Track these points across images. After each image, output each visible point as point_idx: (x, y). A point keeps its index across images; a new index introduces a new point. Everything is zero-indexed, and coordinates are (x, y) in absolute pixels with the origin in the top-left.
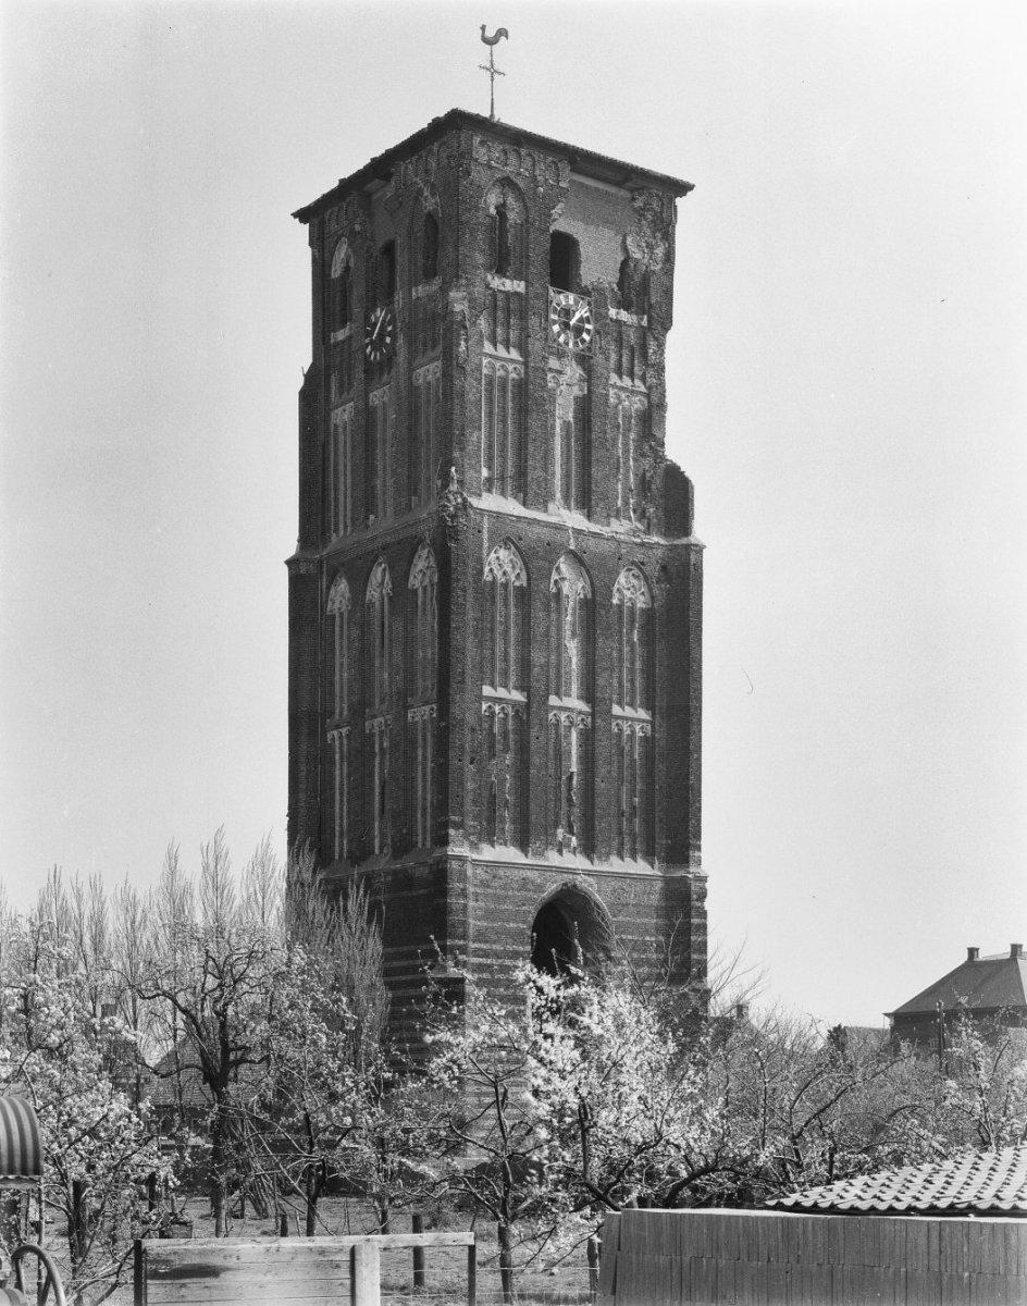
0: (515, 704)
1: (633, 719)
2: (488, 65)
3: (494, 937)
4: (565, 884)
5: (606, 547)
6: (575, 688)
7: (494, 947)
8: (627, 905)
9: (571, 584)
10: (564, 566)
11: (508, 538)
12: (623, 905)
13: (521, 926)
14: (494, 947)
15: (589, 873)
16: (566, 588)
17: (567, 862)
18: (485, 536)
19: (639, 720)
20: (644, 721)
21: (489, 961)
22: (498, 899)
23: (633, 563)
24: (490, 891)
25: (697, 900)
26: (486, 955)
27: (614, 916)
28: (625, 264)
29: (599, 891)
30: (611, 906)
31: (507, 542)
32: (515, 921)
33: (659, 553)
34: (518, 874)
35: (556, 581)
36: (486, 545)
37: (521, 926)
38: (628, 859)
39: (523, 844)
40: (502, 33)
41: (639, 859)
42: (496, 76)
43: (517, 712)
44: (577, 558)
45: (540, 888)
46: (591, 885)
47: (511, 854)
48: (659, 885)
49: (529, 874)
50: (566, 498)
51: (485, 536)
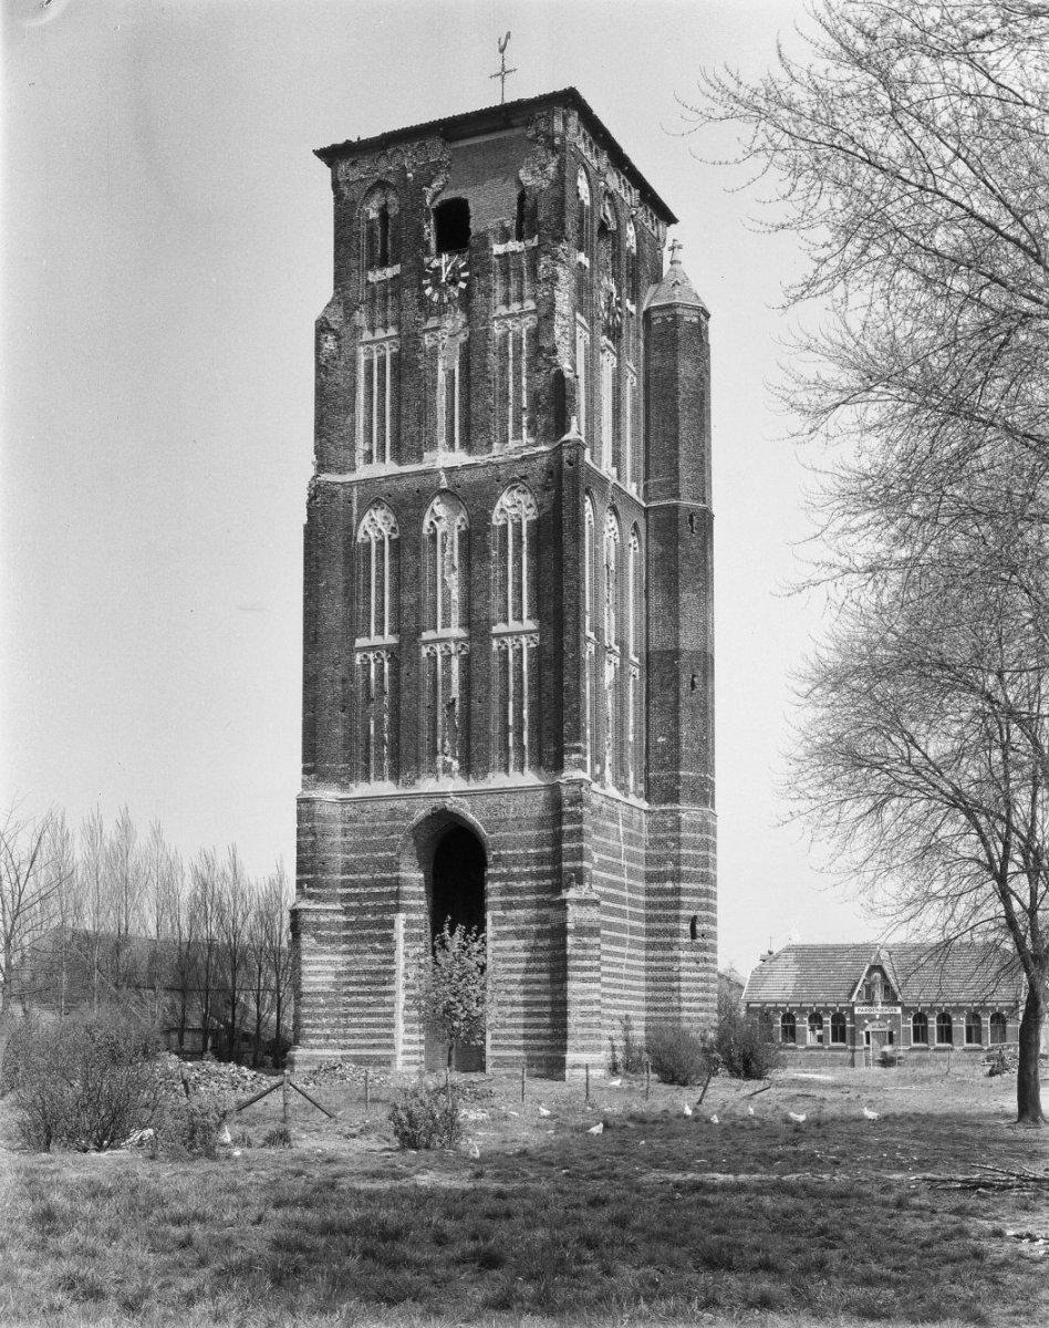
0: (388, 648)
1: (519, 633)
2: (499, 78)
3: (360, 868)
4: (435, 808)
5: (480, 475)
6: (455, 618)
7: (362, 876)
8: (506, 819)
9: (443, 520)
10: (439, 507)
11: (378, 499)
12: (501, 821)
13: (390, 854)
14: (362, 876)
15: (460, 794)
16: (441, 527)
17: (444, 785)
18: (355, 504)
19: (524, 632)
20: (531, 632)
21: (357, 891)
22: (365, 832)
23: (514, 480)
24: (358, 825)
25: (570, 805)
26: (353, 884)
27: (492, 833)
28: (522, 198)
29: (472, 811)
30: (487, 823)
31: (376, 502)
32: (382, 850)
33: (545, 461)
34: (384, 806)
35: (432, 523)
36: (355, 511)
37: (390, 854)
38: (472, 781)
39: (395, 775)
40: (680, 247)
41: (526, 769)
42: (499, 78)
43: (392, 654)
44: (449, 495)
45: (408, 815)
46: (462, 806)
47: (386, 787)
48: (542, 795)
49: (396, 804)
50: (451, 441)
51: (355, 504)
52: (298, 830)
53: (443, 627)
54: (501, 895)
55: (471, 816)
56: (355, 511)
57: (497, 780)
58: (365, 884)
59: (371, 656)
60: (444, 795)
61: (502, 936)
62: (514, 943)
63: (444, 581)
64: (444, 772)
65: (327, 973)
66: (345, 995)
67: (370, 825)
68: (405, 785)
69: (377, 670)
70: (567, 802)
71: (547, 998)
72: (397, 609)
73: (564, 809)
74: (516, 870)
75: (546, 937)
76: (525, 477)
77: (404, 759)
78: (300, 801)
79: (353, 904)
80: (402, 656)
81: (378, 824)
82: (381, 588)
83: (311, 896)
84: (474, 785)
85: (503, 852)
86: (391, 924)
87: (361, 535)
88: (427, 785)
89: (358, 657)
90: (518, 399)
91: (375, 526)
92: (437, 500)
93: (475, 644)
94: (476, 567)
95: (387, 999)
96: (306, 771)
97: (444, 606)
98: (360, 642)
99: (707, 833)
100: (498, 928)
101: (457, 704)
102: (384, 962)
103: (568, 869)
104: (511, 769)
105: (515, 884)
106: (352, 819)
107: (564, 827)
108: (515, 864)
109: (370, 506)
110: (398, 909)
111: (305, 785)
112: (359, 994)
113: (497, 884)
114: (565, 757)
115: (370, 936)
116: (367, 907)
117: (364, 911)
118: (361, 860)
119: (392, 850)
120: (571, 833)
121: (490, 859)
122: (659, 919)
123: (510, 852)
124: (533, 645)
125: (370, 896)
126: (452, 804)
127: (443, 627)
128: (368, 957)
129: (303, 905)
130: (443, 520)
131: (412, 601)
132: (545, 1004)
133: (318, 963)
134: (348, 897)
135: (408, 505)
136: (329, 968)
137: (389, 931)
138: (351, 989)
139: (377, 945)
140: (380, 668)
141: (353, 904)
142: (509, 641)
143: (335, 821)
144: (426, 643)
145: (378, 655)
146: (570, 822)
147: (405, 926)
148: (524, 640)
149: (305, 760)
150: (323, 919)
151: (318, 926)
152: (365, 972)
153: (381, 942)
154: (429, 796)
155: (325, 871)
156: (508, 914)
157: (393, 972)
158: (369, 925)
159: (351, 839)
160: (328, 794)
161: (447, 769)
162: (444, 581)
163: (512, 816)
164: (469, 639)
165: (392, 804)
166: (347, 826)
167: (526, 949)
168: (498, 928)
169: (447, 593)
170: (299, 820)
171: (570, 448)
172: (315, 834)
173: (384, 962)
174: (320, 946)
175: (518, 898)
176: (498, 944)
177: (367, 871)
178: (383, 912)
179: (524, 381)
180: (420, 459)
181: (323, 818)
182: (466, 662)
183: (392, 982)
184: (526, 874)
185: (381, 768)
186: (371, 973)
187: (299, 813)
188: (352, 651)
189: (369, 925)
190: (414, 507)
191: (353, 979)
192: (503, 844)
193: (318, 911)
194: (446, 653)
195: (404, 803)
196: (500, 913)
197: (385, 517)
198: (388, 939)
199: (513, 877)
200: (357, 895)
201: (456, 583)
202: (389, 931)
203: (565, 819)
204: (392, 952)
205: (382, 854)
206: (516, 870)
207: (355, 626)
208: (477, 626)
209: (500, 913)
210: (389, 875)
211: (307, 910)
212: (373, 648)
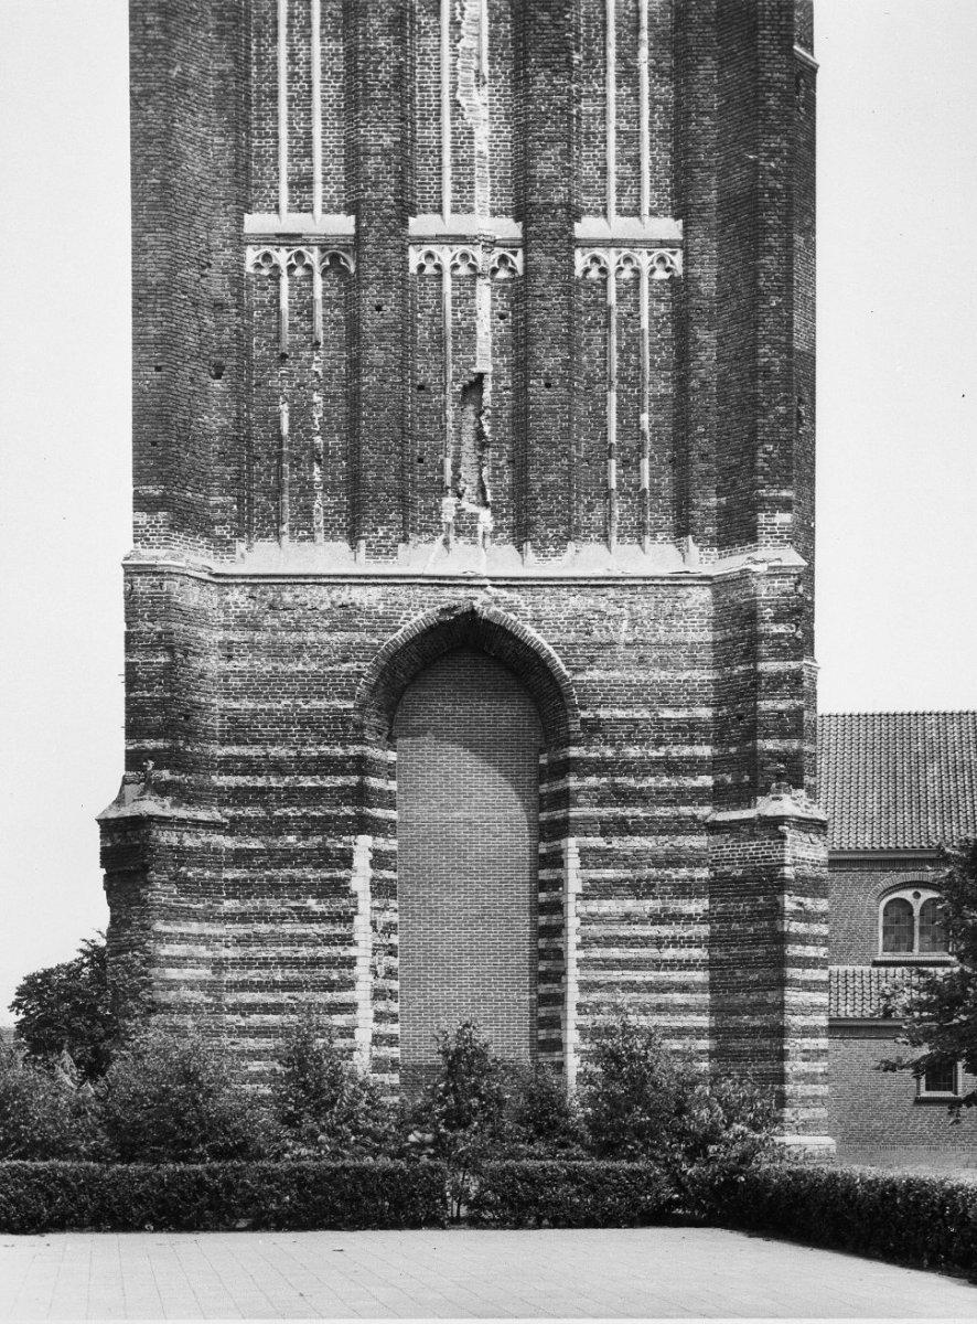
1: (634, 244)
6: (482, 194)
7: (274, 751)
8: (612, 643)
12: (602, 646)
14: (274, 751)
21: (261, 782)
22: (277, 652)
24: (259, 637)
25: (776, 620)
32: (320, 695)
38: (531, 556)
45: (387, 622)
46: (512, 608)
47: (330, 555)
52: (129, 637)
57: (586, 559)
58: (278, 767)
59: (282, 257)
61: (595, 890)
62: (630, 905)
63: (456, 104)
64: (459, 532)
65: (200, 961)
66: (234, 1009)
67: (294, 637)
68: (375, 552)
69: (301, 298)
70: (769, 612)
71: (704, 1021)
72: (353, 155)
73: (762, 628)
74: (633, 752)
75: (700, 895)
77: (380, 492)
78: (132, 571)
79: (249, 812)
80: (366, 264)
81: (311, 637)
83: (162, 789)
84: (532, 565)
85: (603, 713)
86: (346, 860)
88: (423, 557)
89: (251, 255)
93: (539, 257)
94: (541, 81)
95: (339, 1020)
96: (142, 503)
98: (255, 223)
99: (801, 737)
100: (594, 874)
101: (488, 386)
102: (329, 940)
103: (770, 753)
104: (614, 538)
105: (632, 782)
106: (248, 623)
107: (762, 666)
108: (630, 740)
110: (364, 825)
111: (140, 536)
112: (267, 1009)
113: (592, 781)
114: (762, 518)
115: (293, 883)
117: (282, 826)
118: (270, 713)
119: (344, 696)
120: (777, 680)
121: (575, 726)
122: (331, 962)
123: (620, 714)
124: (661, 275)
125: (292, 795)
126: (483, 602)
127: (455, 211)
129: (151, 806)
131: (387, 141)
132: (698, 1033)
133: (183, 938)
134: (240, 796)
136: (202, 951)
137: (341, 874)
138: (248, 997)
139: (312, 903)
140: (302, 290)
141: (249, 812)
142: (611, 258)
143: (205, 624)
144: (421, 241)
145: (300, 255)
146: (777, 656)
147: (373, 864)
148: (644, 260)
149: (140, 475)
150: (189, 842)
151: (182, 855)
152: (283, 963)
153: (319, 896)
155: (190, 734)
156: (616, 843)
157: (350, 963)
158: (289, 857)
159: (243, 665)
160: (190, 556)
162: (456, 104)
163: (624, 637)
164: (525, 244)
166: (235, 637)
167: (706, 918)
168: (594, 874)
169: (464, 137)
170: (131, 615)
172: (170, 650)
173: (329, 940)
174: (185, 902)
175: (639, 812)
176: (594, 907)
177: (281, 739)
178: (324, 831)
181: (189, 616)
182: (519, 293)
183: (349, 985)
184: (656, 762)
185: (307, 512)
186: (296, 963)
187: (131, 599)
188: (239, 241)
189: (289, 857)
191: (252, 975)
192: (608, 697)
193: (182, 822)
194: (463, 270)
195: (376, 593)
196: (597, 842)
198: (339, 888)
199: (627, 767)
201: (484, 113)
202: (341, 874)
203: (763, 650)
204: (348, 919)
205: (322, 704)
206: (633, 752)
207: (246, 189)
208: (541, 214)
209: (597, 842)
210: (339, 751)
211: (164, 821)
212: (287, 239)
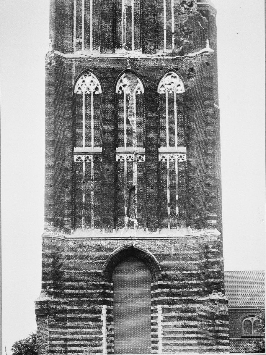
4: (127, 246)
5: (151, 65)
9: (130, 88)
12: (167, 255)
21: (77, 291)
24: (77, 254)
25: (213, 248)
31: (86, 72)
32: (93, 269)
45: (110, 249)
53: (127, 146)
54: (167, 296)
55: (148, 251)
56: (74, 76)
58: (82, 288)
60: (131, 239)
62: (176, 323)
67: (86, 254)
74: (176, 282)
76: (177, 69)
77: (114, 218)
81: (90, 254)
82: (88, 120)
85: (168, 272)
86: (100, 312)
87: (76, 89)
90: (169, 27)
91: (88, 85)
92: (124, 75)
97: (128, 135)
98: (77, 150)
102: (95, 333)
109: (82, 74)
115: (86, 318)
116: (84, 301)
117: (82, 303)
123: (172, 272)
125: (86, 295)
128: (84, 330)
130: (130, 88)
135: (109, 76)
137: (99, 315)
139: (91, 323)
147: (107, 313)
154: (124, 239)
158: (85, 311)
159: (72, 261)
161: (131, 225)
162: (128, 120)
163: (173, 252)
165: (99, 243)
168: (166, 315)
169: (130, 128)
170: (43, 267)
171: (208, 56)
173: (95, 333)
175: (178, 298)
179: (173, 19)
180: (114, 52)
184: (182, 285)
189: (85, 311)
190: (112, 77)
195: (107, 242)
197: (92, 81)
198: (98, 319)
199: (174, 286)
200: (77, 294)
202: (99, 315)
206: (176, 282)
210: (98, 283)
212: (85, 153)
